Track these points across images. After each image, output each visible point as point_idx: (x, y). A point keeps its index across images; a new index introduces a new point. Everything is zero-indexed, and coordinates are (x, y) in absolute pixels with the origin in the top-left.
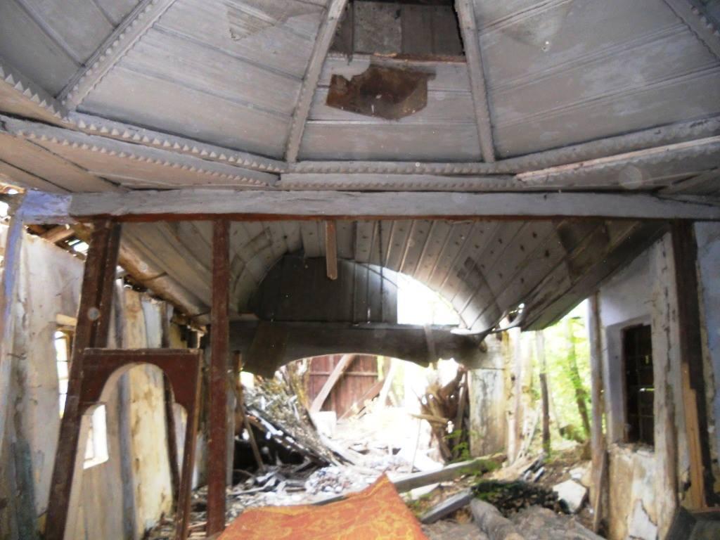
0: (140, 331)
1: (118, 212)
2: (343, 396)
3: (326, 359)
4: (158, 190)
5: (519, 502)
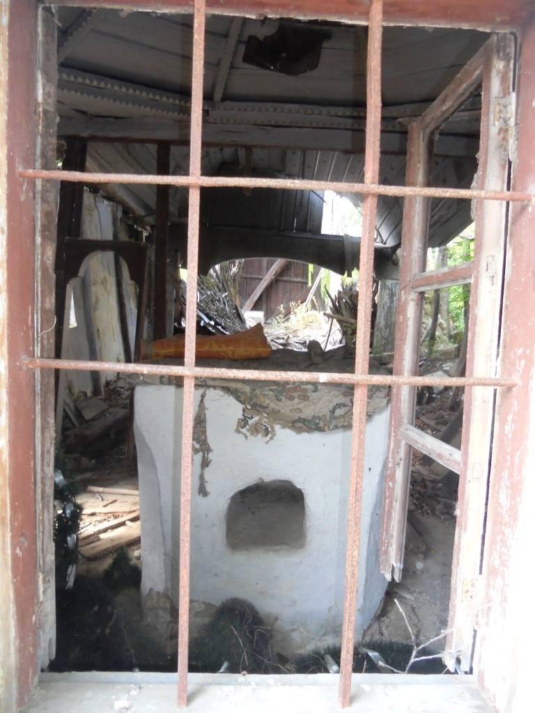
1: (85, 134)
2: (273, 298)
3: (260, 263)
4: (116, 118)
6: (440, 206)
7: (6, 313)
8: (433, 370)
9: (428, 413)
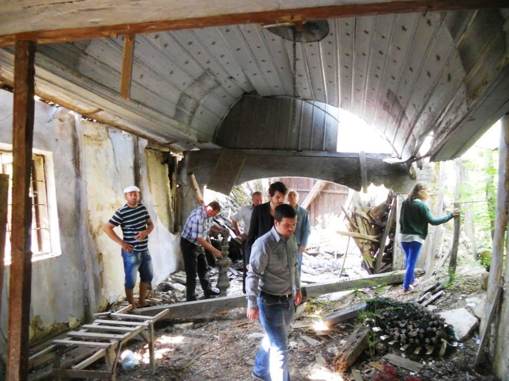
0: (107, 156)
5: (403, 323)
6: (447, 110)
7: (31, 233)
8: (453, 305)
9: (446, 375)
